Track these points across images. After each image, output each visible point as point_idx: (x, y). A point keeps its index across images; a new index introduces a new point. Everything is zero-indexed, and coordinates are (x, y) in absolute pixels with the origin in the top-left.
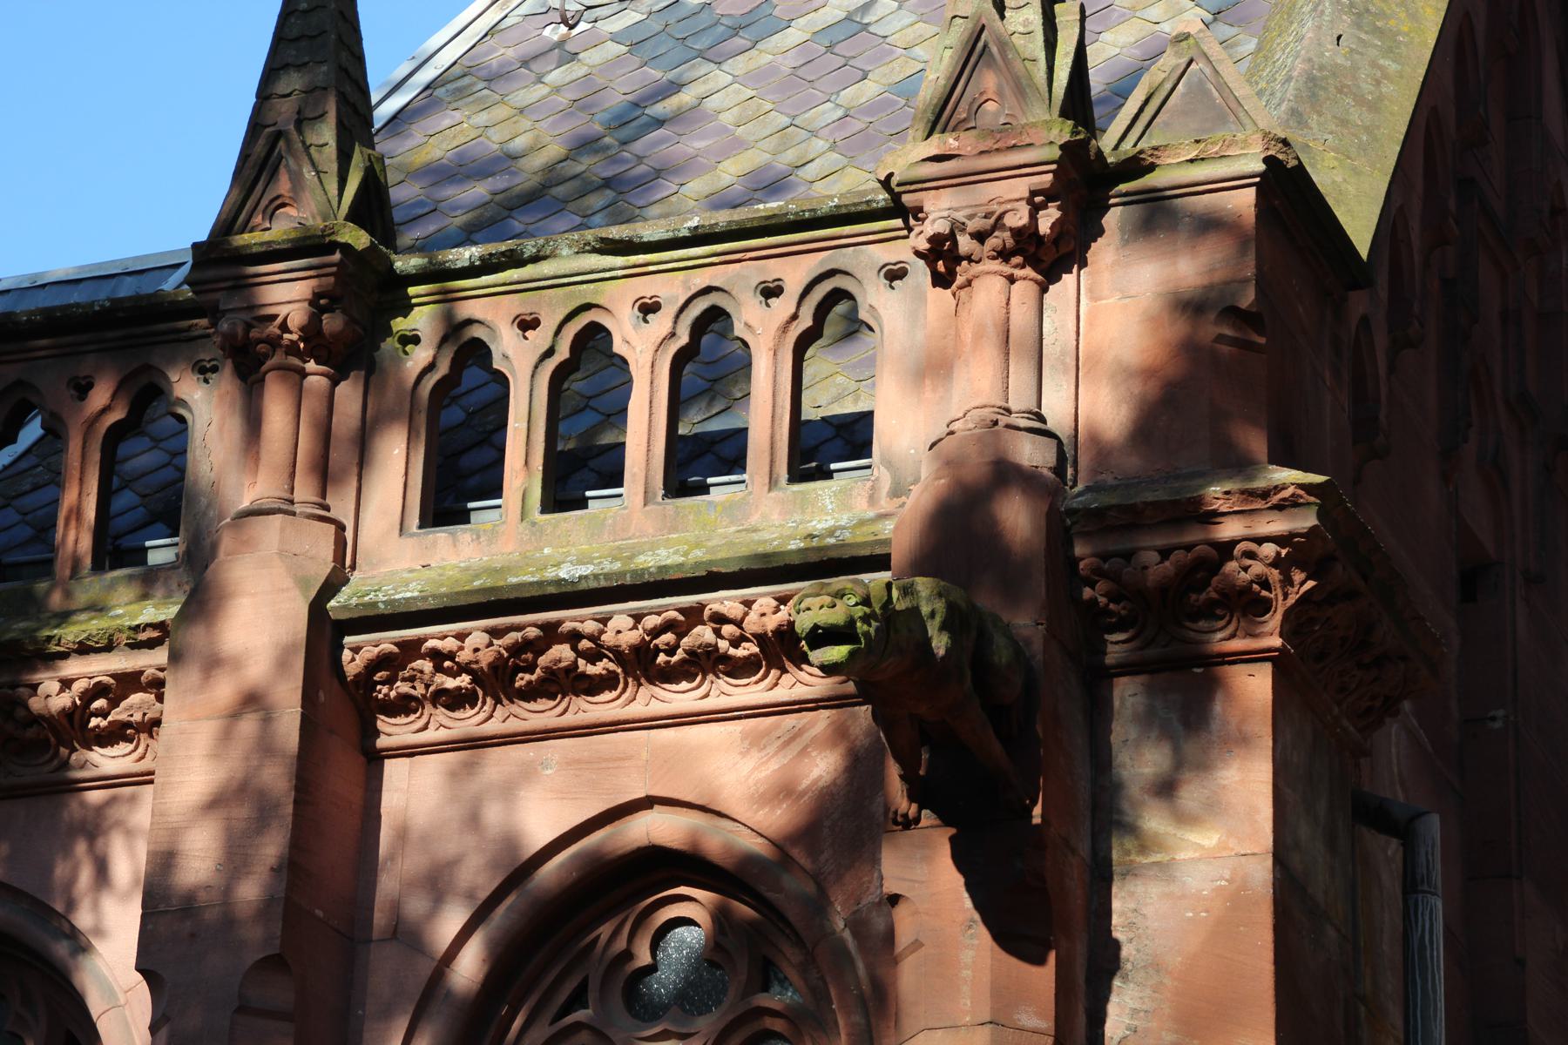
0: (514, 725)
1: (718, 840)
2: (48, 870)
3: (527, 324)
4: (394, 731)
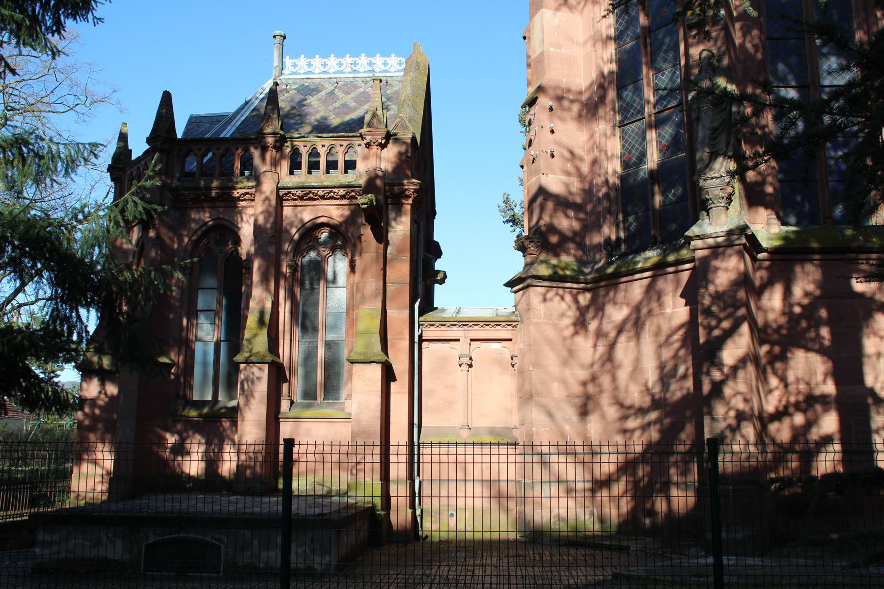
0: (303, 204)
1: (332, 222)
2: (234, 218)
3: (305, 146)
4: (285, 203)
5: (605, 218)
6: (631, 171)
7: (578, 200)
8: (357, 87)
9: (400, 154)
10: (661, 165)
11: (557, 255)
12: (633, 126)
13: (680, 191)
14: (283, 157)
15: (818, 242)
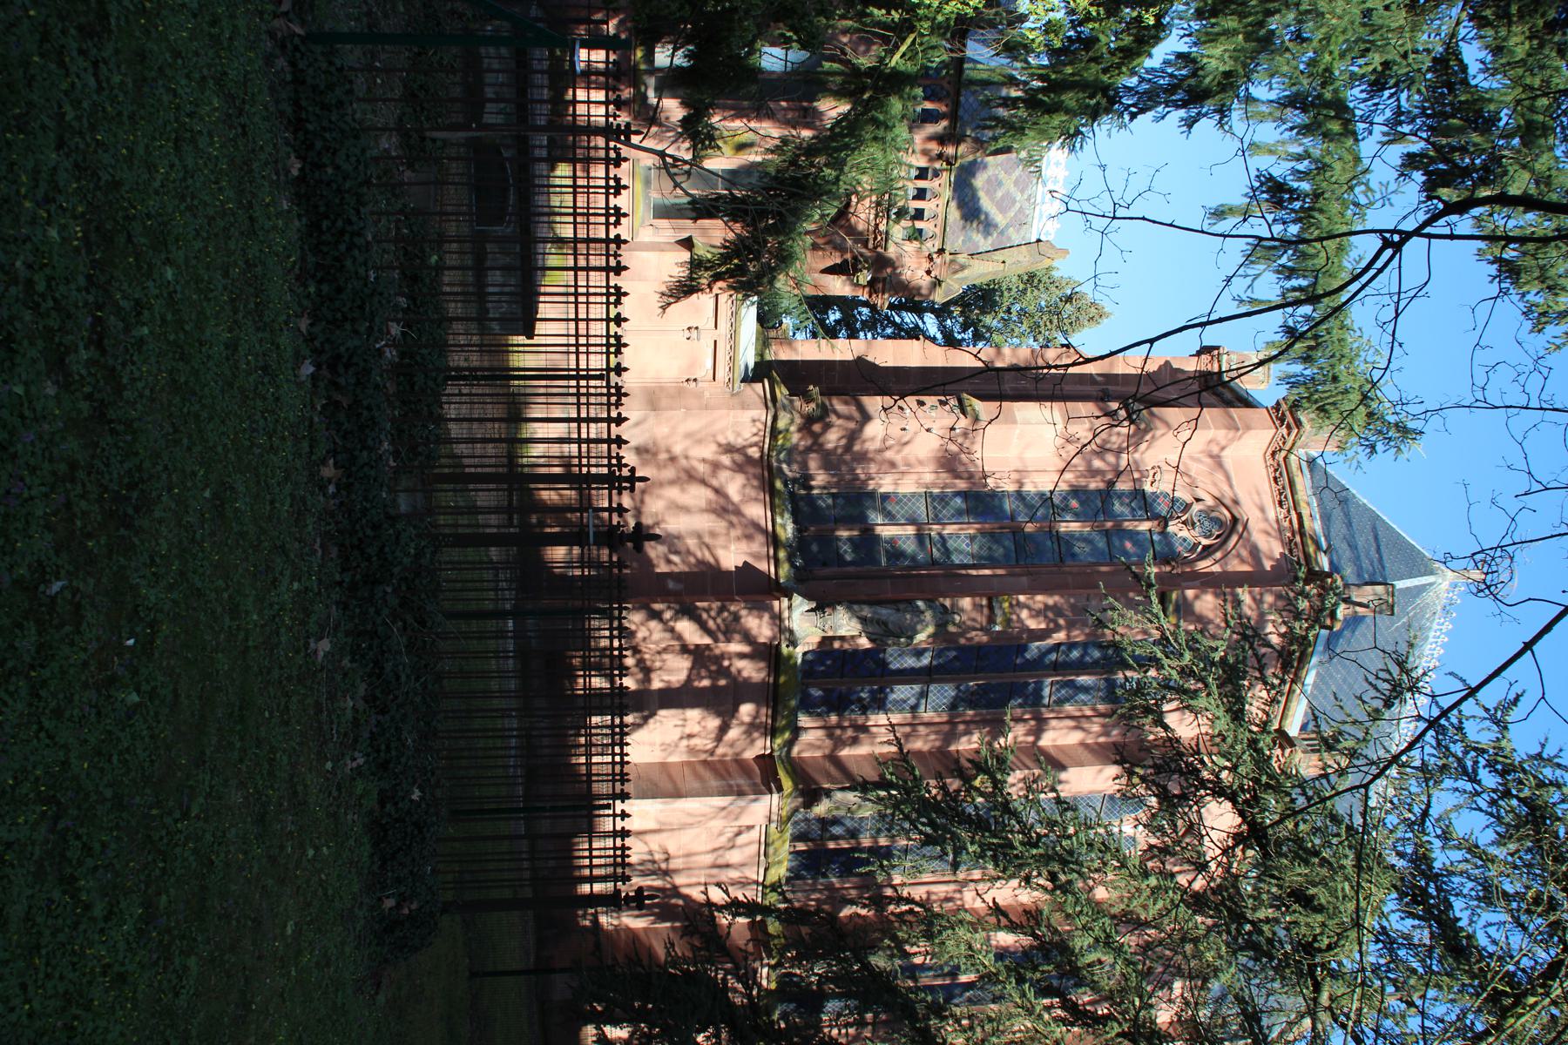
5: (833, 475)
7: (857, 448)
8: (1022, 192)
9: (919, 289)
10: (877, 539)
11: (800, 430)
12: (924, 508)
13: (848, 558)
14: (931, 160)
15: (785, 682)
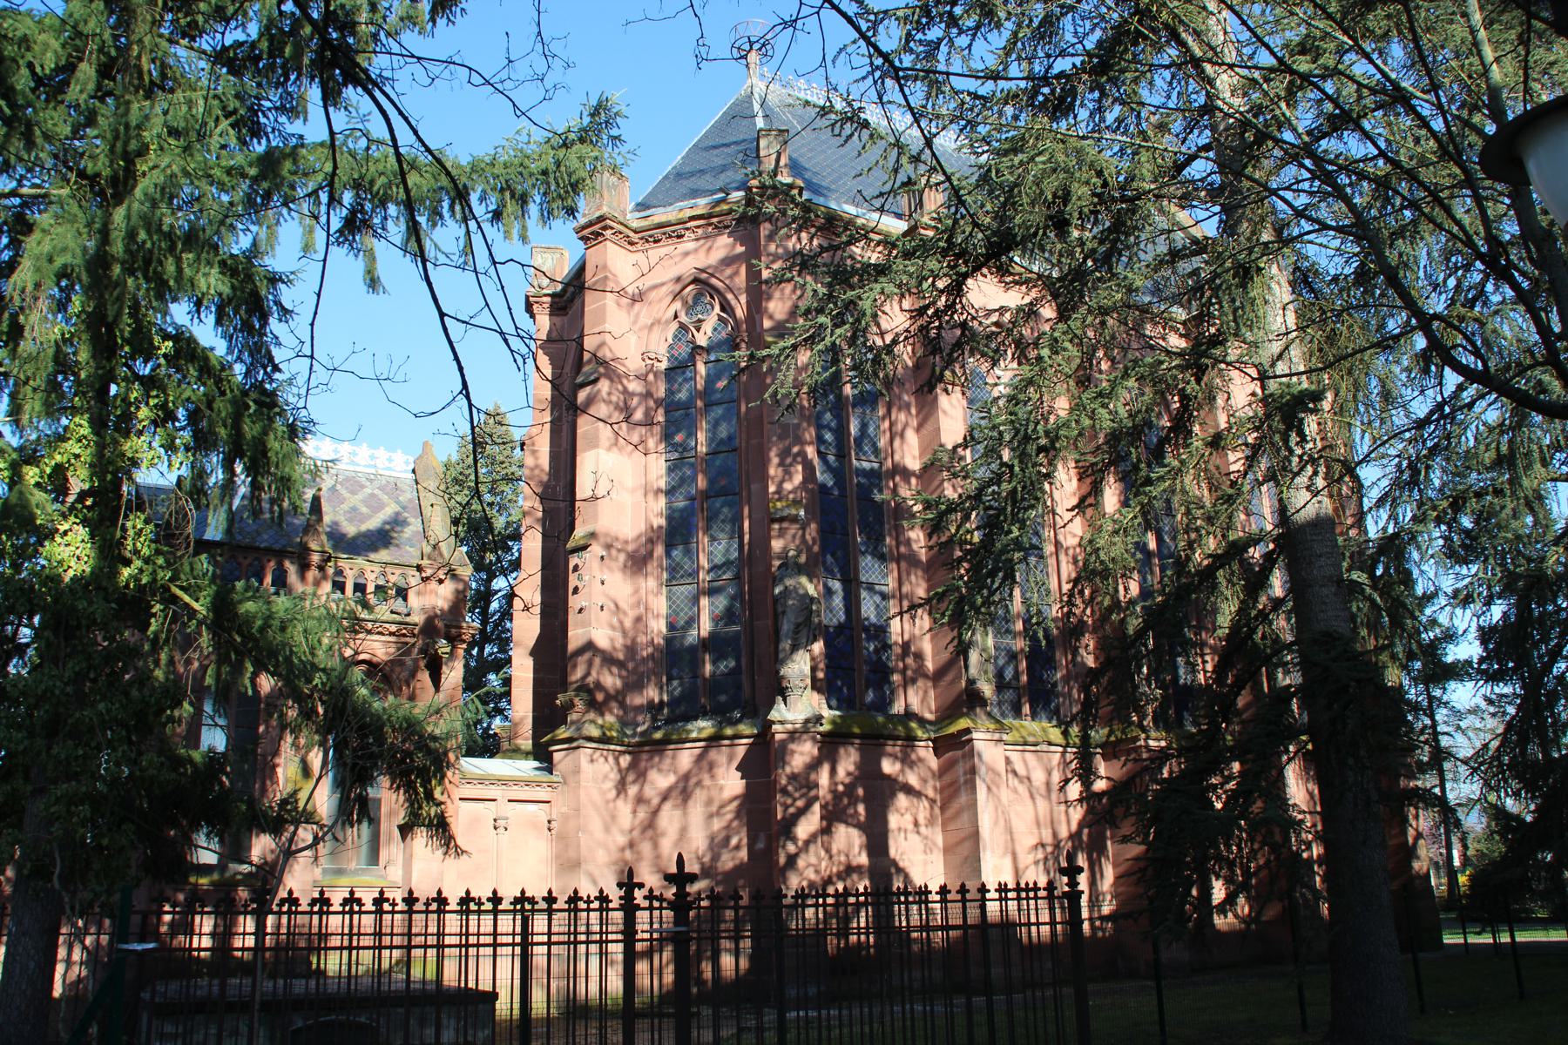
1: (375, 659)
6: (677, 634)
7: (621, 656)
8: (363, 487)
10: (712, 635)
11: (602, 715)
12: (682, 588)
13: (732, 664)
14: (325, 577)
